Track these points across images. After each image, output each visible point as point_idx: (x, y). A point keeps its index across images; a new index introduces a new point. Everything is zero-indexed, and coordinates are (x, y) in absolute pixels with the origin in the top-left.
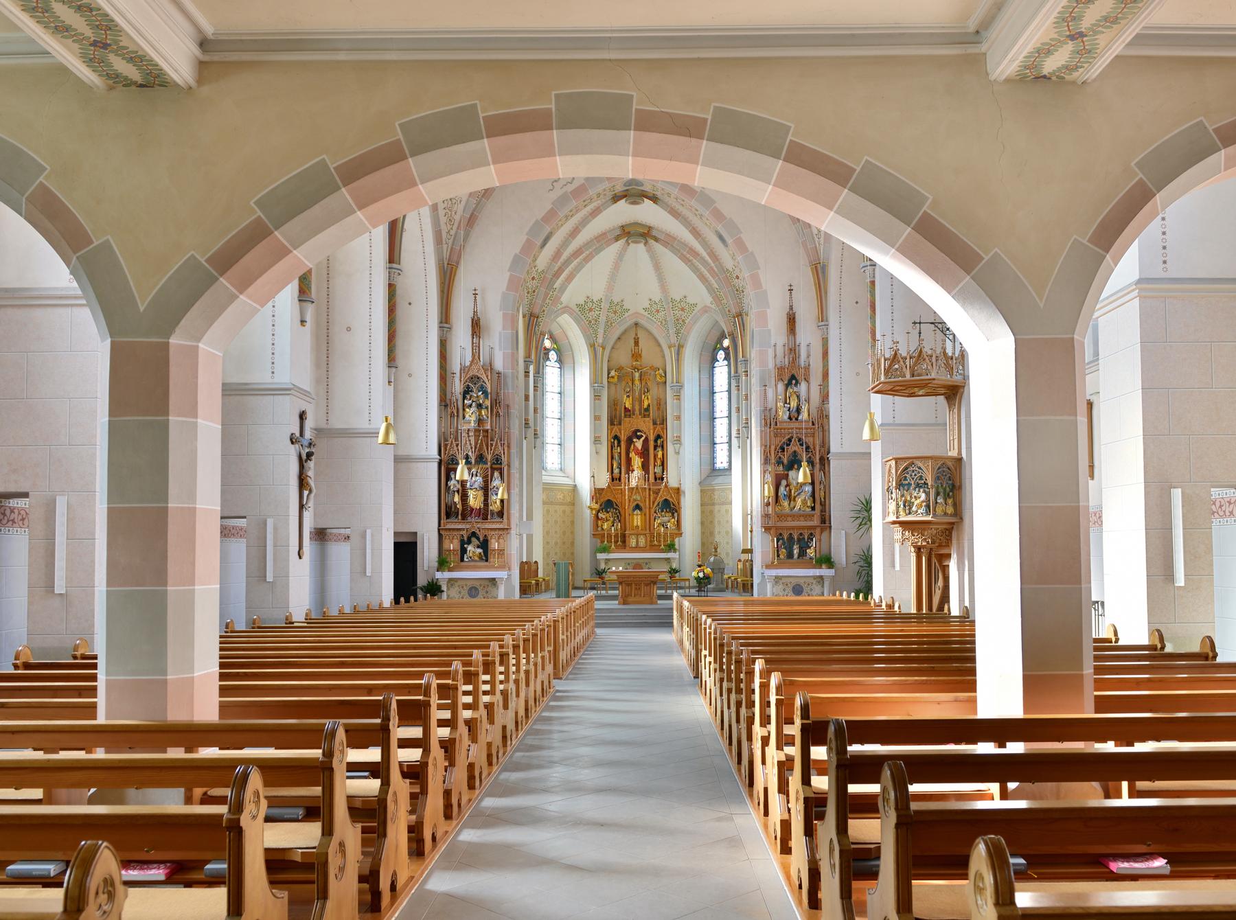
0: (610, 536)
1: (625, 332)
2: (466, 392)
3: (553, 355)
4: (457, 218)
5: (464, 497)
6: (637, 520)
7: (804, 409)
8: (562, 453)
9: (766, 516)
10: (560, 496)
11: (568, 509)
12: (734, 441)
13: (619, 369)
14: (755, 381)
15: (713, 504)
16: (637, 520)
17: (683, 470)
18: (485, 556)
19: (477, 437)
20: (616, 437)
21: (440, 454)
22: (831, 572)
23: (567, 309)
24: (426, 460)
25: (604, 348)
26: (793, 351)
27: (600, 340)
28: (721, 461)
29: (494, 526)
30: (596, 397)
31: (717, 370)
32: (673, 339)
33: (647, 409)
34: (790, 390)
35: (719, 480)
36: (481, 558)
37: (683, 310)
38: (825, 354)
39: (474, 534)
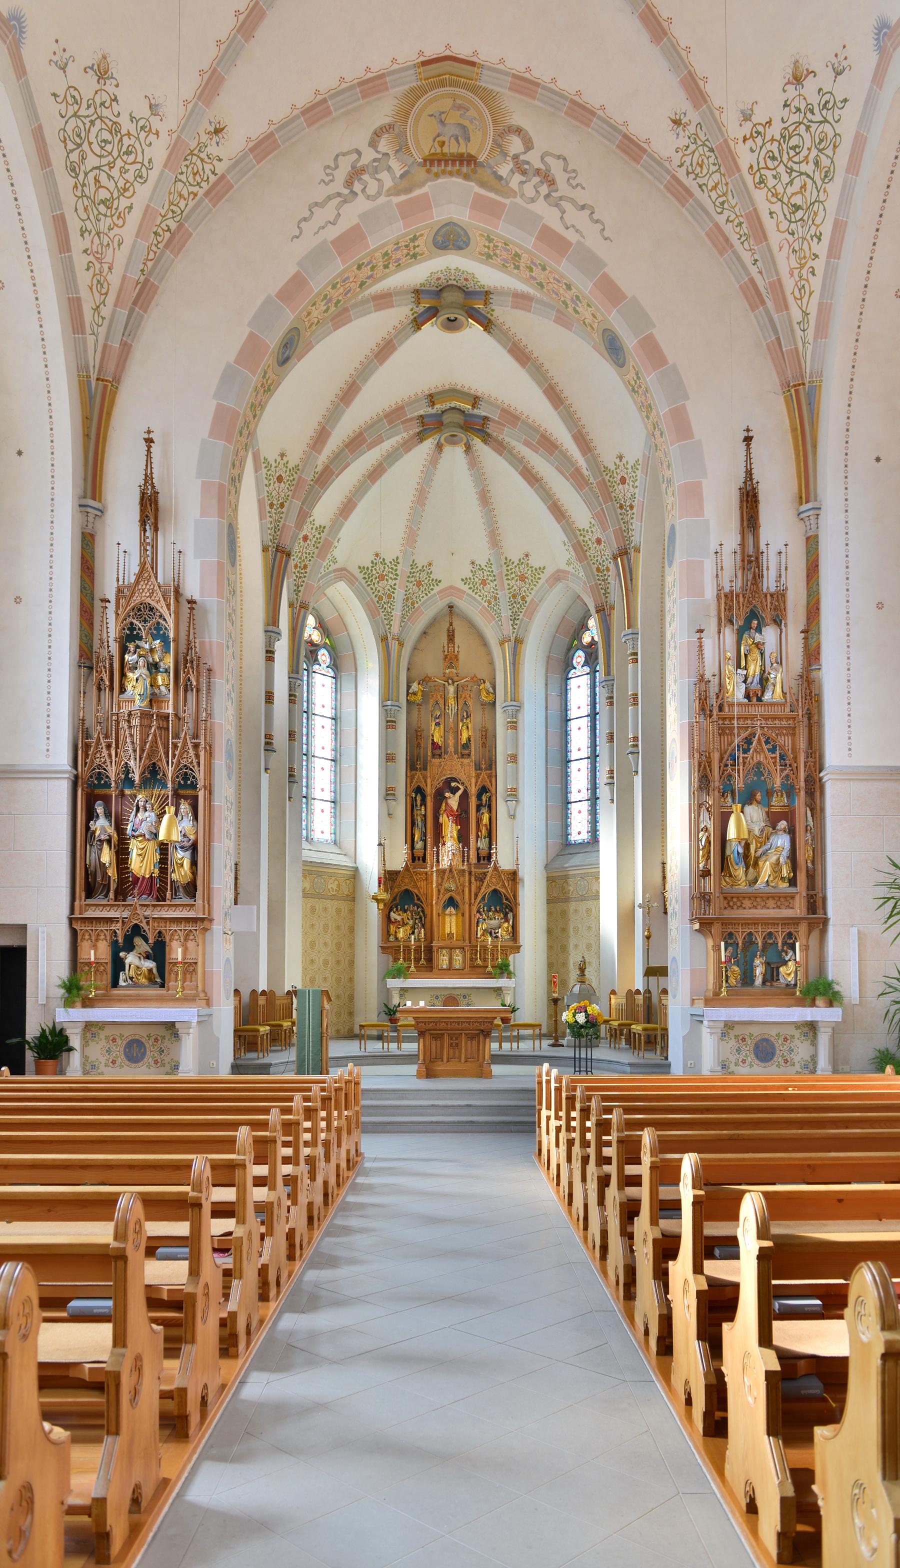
0: (407, 950)
1: (434, 623)
2: (129, 637)
3: (323, 656)
4: (114, 279)
5: (122, 854)
6: (451, 924)
7: (777, 677)
8: (336, 815)
9: (701, 898)
10: (332, 885)
11: (344, 906)
12: (603, 792)
13: (425, 681)
14: (677, 634)
15: (567, 900)
16: (451, 924)
17: (520, 844)
18: (160, 976)
19: (145, 727)
20: (419, 790)
21: (75, 766)
22: (833, 1015)
23: (343, 574)
24: (46, 774)
25: (401, 645)
26: (751, 561)
27: (395, 629)
28: (579, 829)
29: (178, 914)
30: (388, 723)
31: (573, 683)
32: (508, 630)
33: (466, 746)
34: (747, 641)
35: (576, 860)
36: (151, 980)
37: (523, 578)
38: (813, 570)
39: (136, 930)
